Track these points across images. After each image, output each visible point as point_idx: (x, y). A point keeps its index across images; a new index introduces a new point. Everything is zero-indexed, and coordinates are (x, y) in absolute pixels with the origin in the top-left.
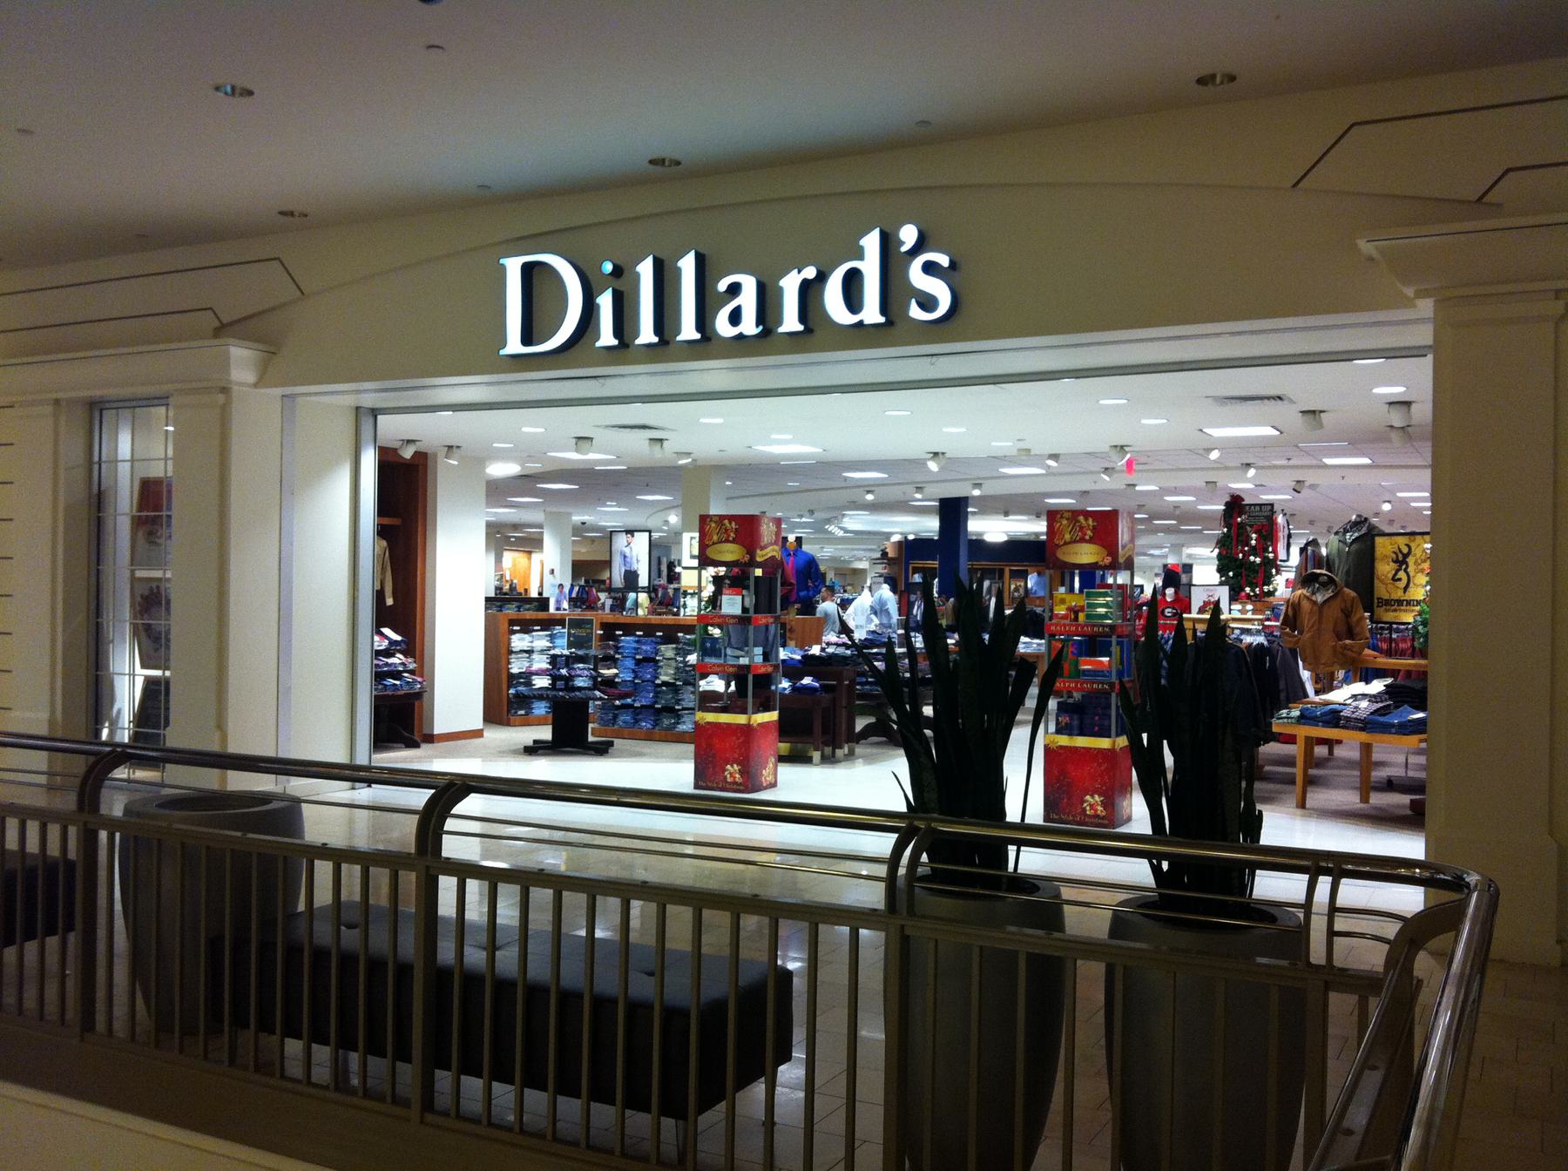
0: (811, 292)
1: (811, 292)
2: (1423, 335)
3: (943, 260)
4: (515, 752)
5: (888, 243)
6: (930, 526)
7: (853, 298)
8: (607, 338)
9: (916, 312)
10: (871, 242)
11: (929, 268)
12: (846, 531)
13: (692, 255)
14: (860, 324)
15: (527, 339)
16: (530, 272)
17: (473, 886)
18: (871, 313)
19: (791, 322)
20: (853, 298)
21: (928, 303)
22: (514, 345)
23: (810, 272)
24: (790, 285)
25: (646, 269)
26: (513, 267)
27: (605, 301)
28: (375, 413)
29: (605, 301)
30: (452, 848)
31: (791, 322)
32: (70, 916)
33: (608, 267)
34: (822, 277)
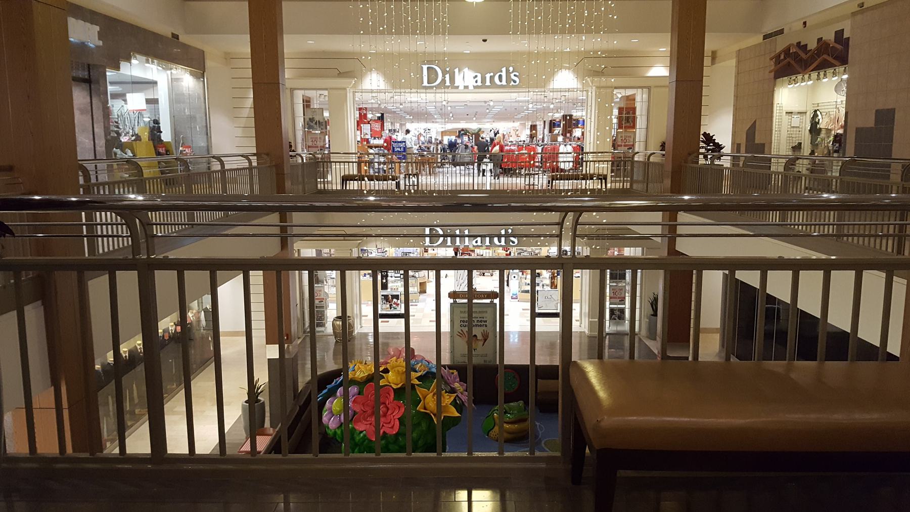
1: (492, 78)
5: (507, 71)
7: (501, 80)
8: (448, 84)
9: (512, 83)
10: (504, 70)
18: (504, 83)
19: (488, 83)
20: (501, 80)
22: (425, 83)
24: (488, 76)
26: (425, 67)
31: (488, 83)
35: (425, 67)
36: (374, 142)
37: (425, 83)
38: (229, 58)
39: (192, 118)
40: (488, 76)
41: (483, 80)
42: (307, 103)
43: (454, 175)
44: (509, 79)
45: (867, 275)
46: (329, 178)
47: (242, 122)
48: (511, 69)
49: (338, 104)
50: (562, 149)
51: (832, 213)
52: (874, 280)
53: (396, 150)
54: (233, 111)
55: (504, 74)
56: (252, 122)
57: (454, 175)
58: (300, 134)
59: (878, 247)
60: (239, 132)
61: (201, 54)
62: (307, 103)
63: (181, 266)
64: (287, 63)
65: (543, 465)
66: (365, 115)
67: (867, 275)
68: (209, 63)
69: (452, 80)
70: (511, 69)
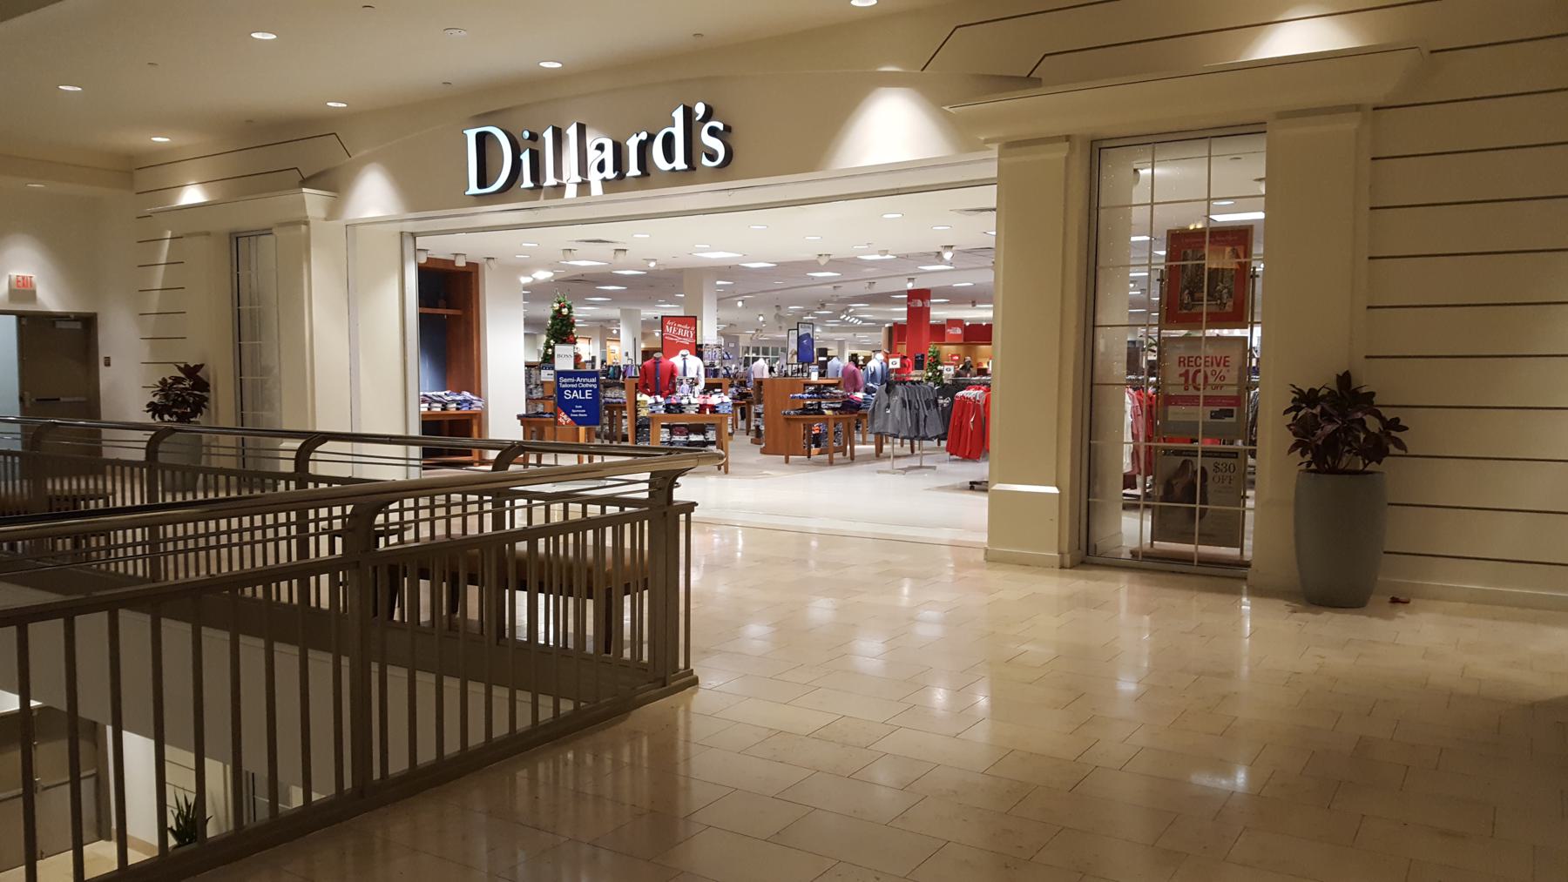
0: (644, 148)
1: (644, 148)
2: (992, 171)
3: (720, 126)
4: (962, 489)
5: (688, 113)
6: (900, 314)
7: (669, 156)
8: (527, 182)
9: (705, 162)
10: (678, 115)
11: (713, 132)
12: (864, 320)
13: (574, 126)
14: (674, 170)
15: (482, 183)
16: (482, 139)
17: (178, 474)
18: (680, 163)
19: (633, 170)
20: (669, 156)
21: (712, 156)
22: (473, 189)
23: (644, 136)
24: (632, 144)
25: (548, 135)
26: (471, 135)
27: (525, 157)
28: (414, 236)
29: (525, 157)
30: (162, 458)
31: (633, 170)
32: (571, 586)
33: (526, 134)
34: (651, 138)
45: (34, 629)
48: (700, 109)
53: (1211, 380)
55: (678, 132)
59: (131, 571)
63: (530, 496)
65: (681, 665)
66: (925, 311)
67: (34, 629)
70: (700, 109)
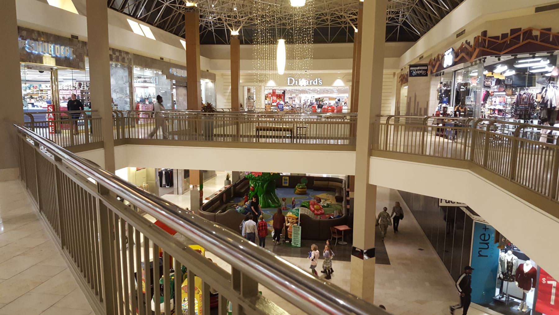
1: (312, 82)
22: (289, 84)
24: (311, 82)
26: (289, 79)
35: (289, 79)
36: (273, 104)
37: (289, 84)
38: (223, 75)
39: (211, 96)
40: (311, 82)
41: (309, 83)
42: (249, 90)
43: (149, 125)
44: (318, 83)
46: (333, 103)
47: (228, 94)
49: (259, 91)
50: (344, 108)
51: (418, 133)
52: (398, 150)
54: (224, 94)
55: (316, 81)
56: (230, 98)
57: (149, 125)
58: (245, 102)
60: (225, 101)
61: (215, 75)
62: (249, 90)
64: (241, 77)
68: (217, 78)
69: (298, 83)
